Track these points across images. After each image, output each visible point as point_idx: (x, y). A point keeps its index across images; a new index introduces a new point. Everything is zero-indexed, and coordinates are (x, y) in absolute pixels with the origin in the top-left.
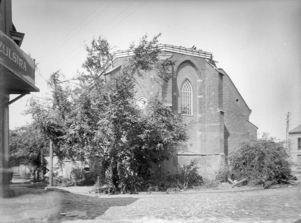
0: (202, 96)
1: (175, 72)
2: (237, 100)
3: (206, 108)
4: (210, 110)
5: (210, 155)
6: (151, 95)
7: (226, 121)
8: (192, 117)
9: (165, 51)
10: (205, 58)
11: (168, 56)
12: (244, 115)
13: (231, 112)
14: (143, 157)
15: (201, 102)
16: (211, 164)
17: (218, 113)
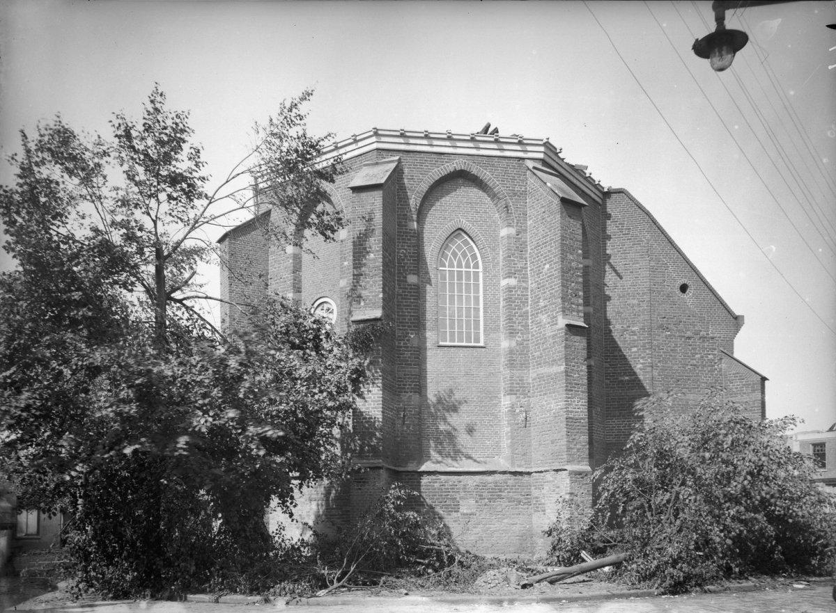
0: (513, 282)
1: (413, 210)
2: (684, 288)
3: (530, 317)
4: (539, 324)
5: (541, 472)
6: (342, 288)
7: (643, 358)
8: (481, 349)
9: (377, 149)
10: (523, 159)
11: (538, 174)
12: (711, 335)
13: (661, 327)
14: (162, 481)
15: (511, 298)
16: (544, 504)
17: (559, 330)
